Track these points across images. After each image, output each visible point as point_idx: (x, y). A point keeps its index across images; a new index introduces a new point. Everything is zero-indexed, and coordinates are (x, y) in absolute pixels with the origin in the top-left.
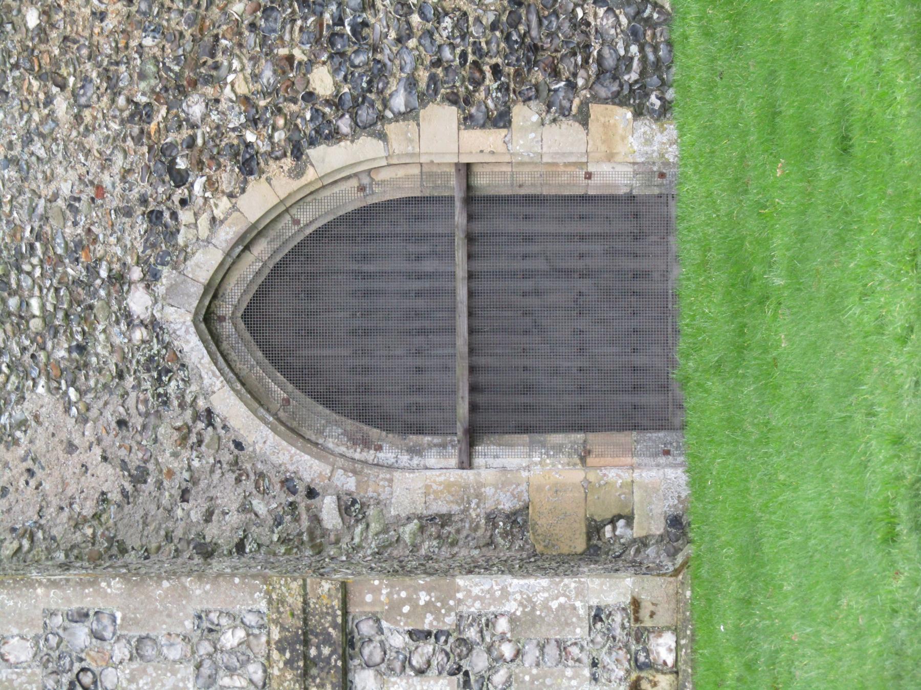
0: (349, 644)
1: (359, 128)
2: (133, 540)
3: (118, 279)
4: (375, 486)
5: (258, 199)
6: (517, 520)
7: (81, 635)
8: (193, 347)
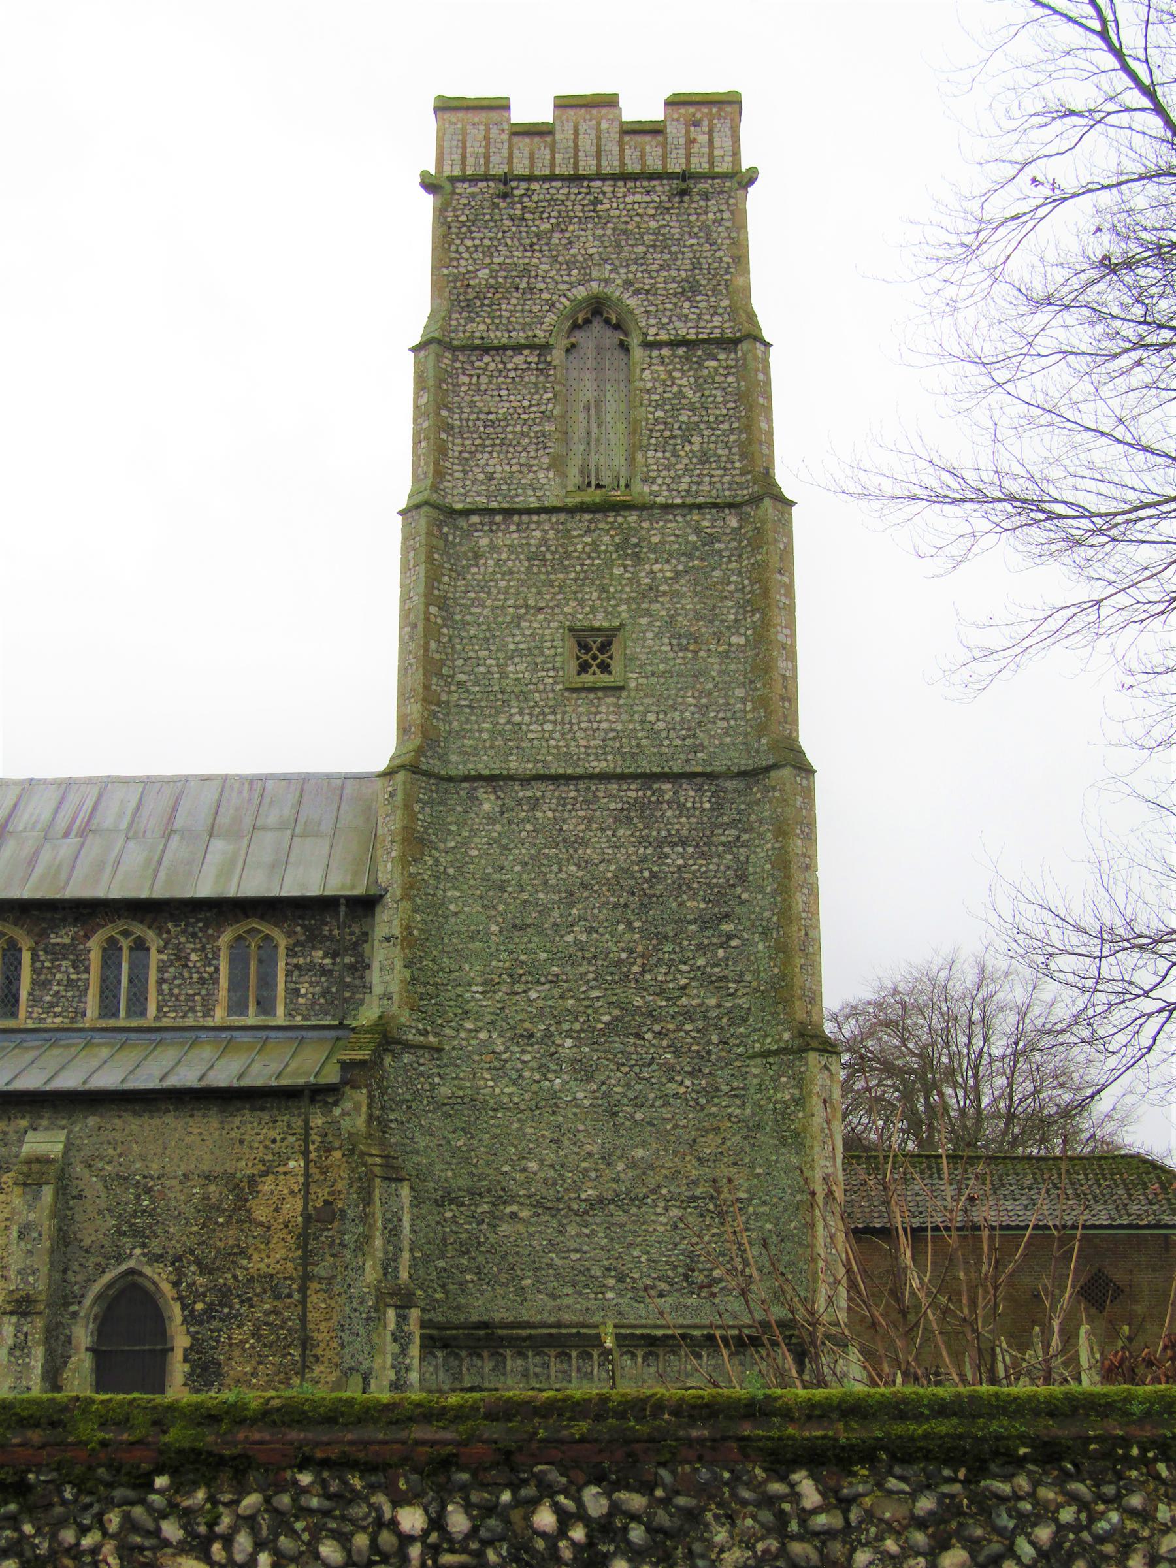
0: (25, 1314)
1: (185, 1317)
2: (69, 1249)
3: (144, 1245)
4: (81, 1322)
5: (166, 1287)
7: (35, 1235)
8: (124, 1267)
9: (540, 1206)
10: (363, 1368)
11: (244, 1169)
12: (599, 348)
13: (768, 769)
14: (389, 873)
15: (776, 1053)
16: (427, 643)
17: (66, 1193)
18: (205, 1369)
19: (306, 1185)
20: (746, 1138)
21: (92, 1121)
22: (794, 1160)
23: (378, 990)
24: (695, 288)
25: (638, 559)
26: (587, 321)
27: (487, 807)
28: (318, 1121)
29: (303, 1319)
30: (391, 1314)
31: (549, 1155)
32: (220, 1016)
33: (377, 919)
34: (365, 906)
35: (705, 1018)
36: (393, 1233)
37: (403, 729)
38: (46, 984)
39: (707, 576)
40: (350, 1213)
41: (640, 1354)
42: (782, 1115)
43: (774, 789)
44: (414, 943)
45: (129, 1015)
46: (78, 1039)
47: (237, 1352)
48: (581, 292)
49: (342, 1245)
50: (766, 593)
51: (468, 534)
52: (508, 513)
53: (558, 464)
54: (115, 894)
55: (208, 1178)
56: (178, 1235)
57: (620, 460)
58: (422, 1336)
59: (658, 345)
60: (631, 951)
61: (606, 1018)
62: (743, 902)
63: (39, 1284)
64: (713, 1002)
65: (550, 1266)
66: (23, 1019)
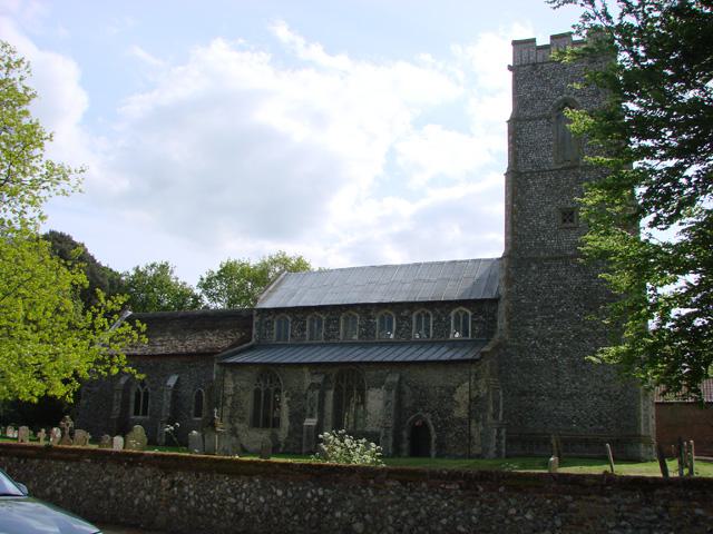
28: (474, 370)
34: (495, 301)
55: (442, 387)
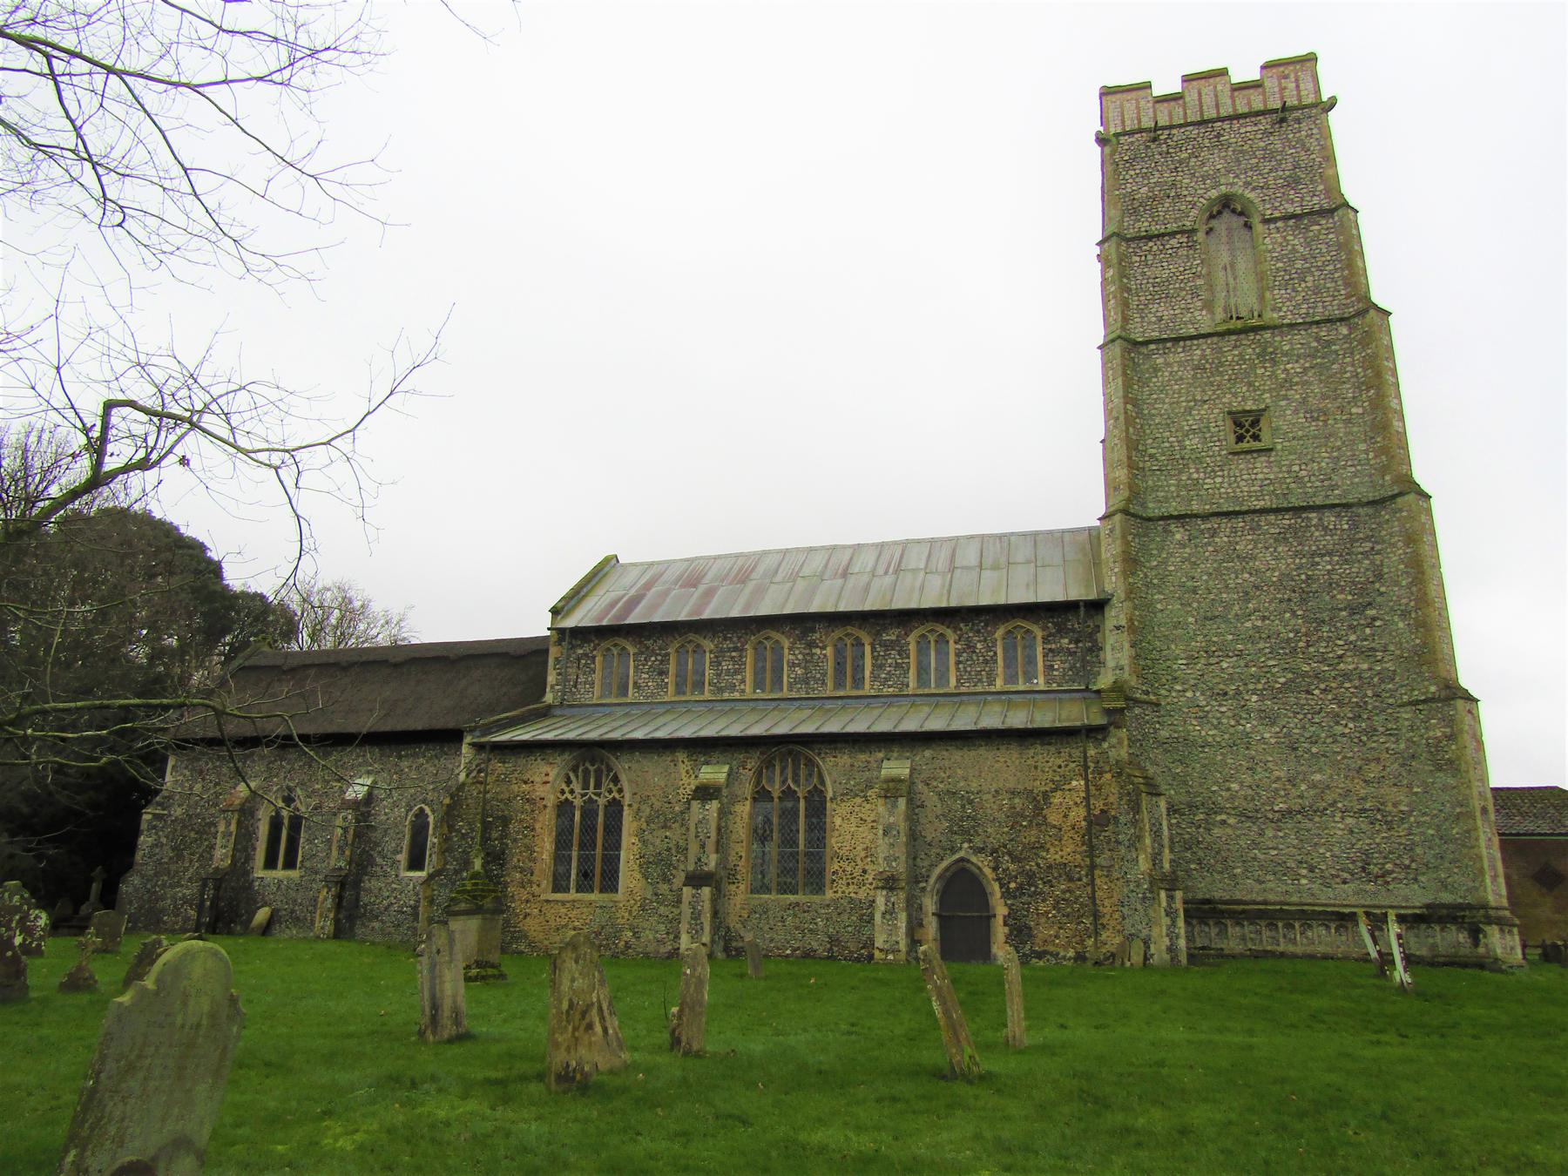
0: (891, 889)
3: (970, 841)
5: (987, 871)
6: (921, 925)
8: (957, 856)
9: (1244, 815)
10: (1142, 935)
11: (1040, 787)
12: (1229, 230)
13: (1394, 497)
14: (1113, 582)
15: (1424, 701)
16: (1127, 431)
17: (914, 806)
18: (1020, 931)
19: (1087, 799)
20: (1403, 765)
21: (928, 753)
22: (1452, 781)
23: (1111, 664)
24: (1297, 181)
25: (1274, 362)
26: (1220, 213)
27: (1178, 536)
29: (1093, 898)
30: (1163, 894)
31: (1248, 780)
32: (999, 684)
33: (1107, 615)
34: (1097, 606)
35: (1360, 678)
36: (1157, 834)
37: (1111, 486)
38: (881, 667)
39: (1328, 369)
40: (1122, 819)
41: (1333, 926)
42: (1435, 748)
43: (1401, 510)
44: (1138, 631)
45: (937, 687)
46: (904, 701)
47: (1043, 920)
48: (1214, 194)
49: (1118, 842)
50: (1378, 375)
51: (1148, 357)
52: (1176, 340)
53: (1209, 306)
54: (925, 605)
56: (994, 834)
57: (1252, 301)
58: (1186, 911)
59: (1274, 220)
60: (1297, 632)
61: (1282, 680)
62: (1382, 594)
63: (900, 867)
64: (1365, 666)
65: (1255, 859)
66: (868, 689)
